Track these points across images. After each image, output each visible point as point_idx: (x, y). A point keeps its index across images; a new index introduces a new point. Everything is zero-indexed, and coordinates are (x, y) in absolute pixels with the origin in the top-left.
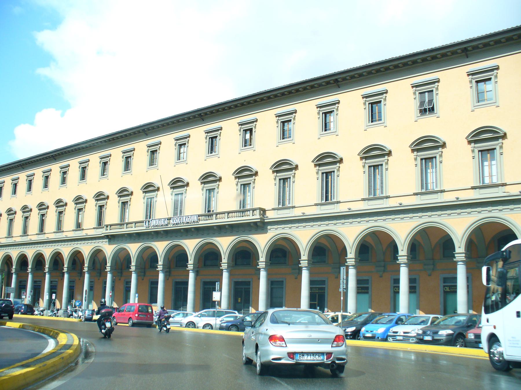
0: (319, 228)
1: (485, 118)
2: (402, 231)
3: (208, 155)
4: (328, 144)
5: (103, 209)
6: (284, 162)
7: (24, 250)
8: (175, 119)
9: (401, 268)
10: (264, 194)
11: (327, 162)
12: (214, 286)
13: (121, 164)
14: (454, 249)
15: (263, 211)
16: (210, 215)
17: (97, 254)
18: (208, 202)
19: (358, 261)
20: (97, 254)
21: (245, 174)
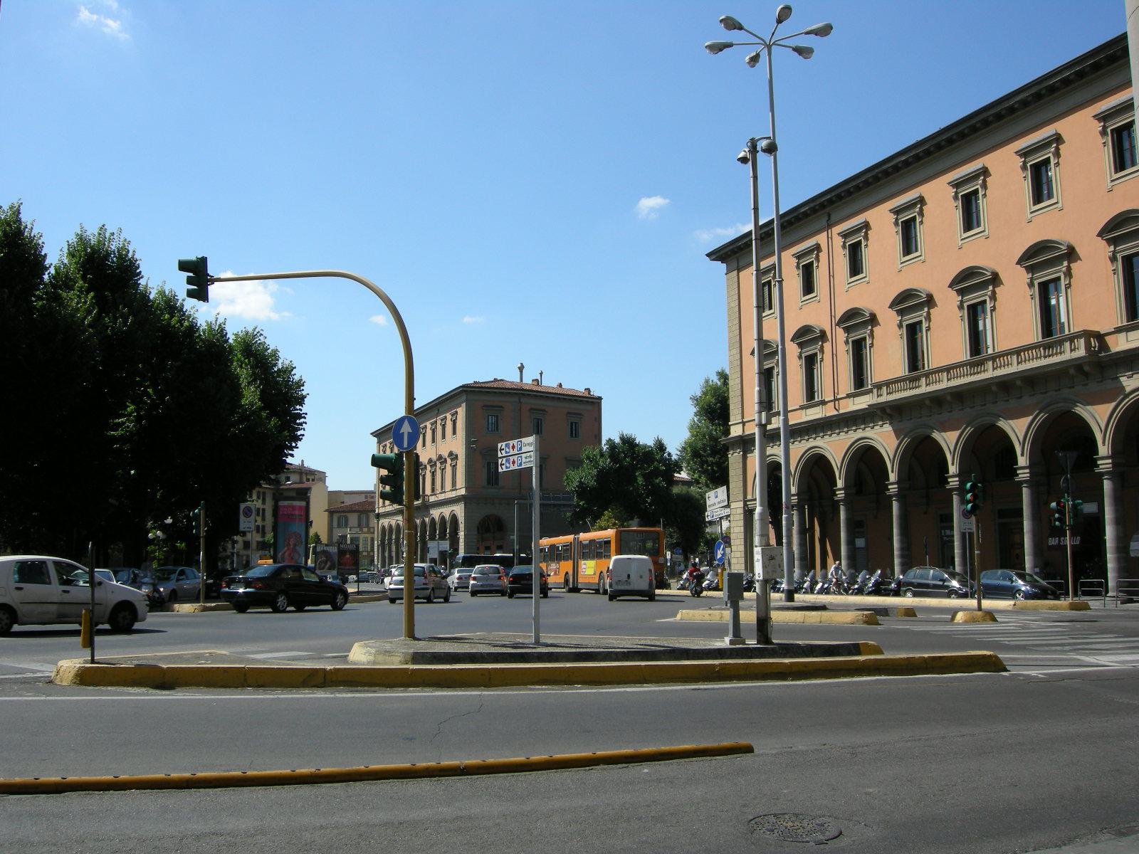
6: (852, 314)
7: (869, 433)
8: (833, 194)
11: (1046, 259)
13: (894, 239)
16: (981, 363)
17: (866, 458)
20: (866, 458)
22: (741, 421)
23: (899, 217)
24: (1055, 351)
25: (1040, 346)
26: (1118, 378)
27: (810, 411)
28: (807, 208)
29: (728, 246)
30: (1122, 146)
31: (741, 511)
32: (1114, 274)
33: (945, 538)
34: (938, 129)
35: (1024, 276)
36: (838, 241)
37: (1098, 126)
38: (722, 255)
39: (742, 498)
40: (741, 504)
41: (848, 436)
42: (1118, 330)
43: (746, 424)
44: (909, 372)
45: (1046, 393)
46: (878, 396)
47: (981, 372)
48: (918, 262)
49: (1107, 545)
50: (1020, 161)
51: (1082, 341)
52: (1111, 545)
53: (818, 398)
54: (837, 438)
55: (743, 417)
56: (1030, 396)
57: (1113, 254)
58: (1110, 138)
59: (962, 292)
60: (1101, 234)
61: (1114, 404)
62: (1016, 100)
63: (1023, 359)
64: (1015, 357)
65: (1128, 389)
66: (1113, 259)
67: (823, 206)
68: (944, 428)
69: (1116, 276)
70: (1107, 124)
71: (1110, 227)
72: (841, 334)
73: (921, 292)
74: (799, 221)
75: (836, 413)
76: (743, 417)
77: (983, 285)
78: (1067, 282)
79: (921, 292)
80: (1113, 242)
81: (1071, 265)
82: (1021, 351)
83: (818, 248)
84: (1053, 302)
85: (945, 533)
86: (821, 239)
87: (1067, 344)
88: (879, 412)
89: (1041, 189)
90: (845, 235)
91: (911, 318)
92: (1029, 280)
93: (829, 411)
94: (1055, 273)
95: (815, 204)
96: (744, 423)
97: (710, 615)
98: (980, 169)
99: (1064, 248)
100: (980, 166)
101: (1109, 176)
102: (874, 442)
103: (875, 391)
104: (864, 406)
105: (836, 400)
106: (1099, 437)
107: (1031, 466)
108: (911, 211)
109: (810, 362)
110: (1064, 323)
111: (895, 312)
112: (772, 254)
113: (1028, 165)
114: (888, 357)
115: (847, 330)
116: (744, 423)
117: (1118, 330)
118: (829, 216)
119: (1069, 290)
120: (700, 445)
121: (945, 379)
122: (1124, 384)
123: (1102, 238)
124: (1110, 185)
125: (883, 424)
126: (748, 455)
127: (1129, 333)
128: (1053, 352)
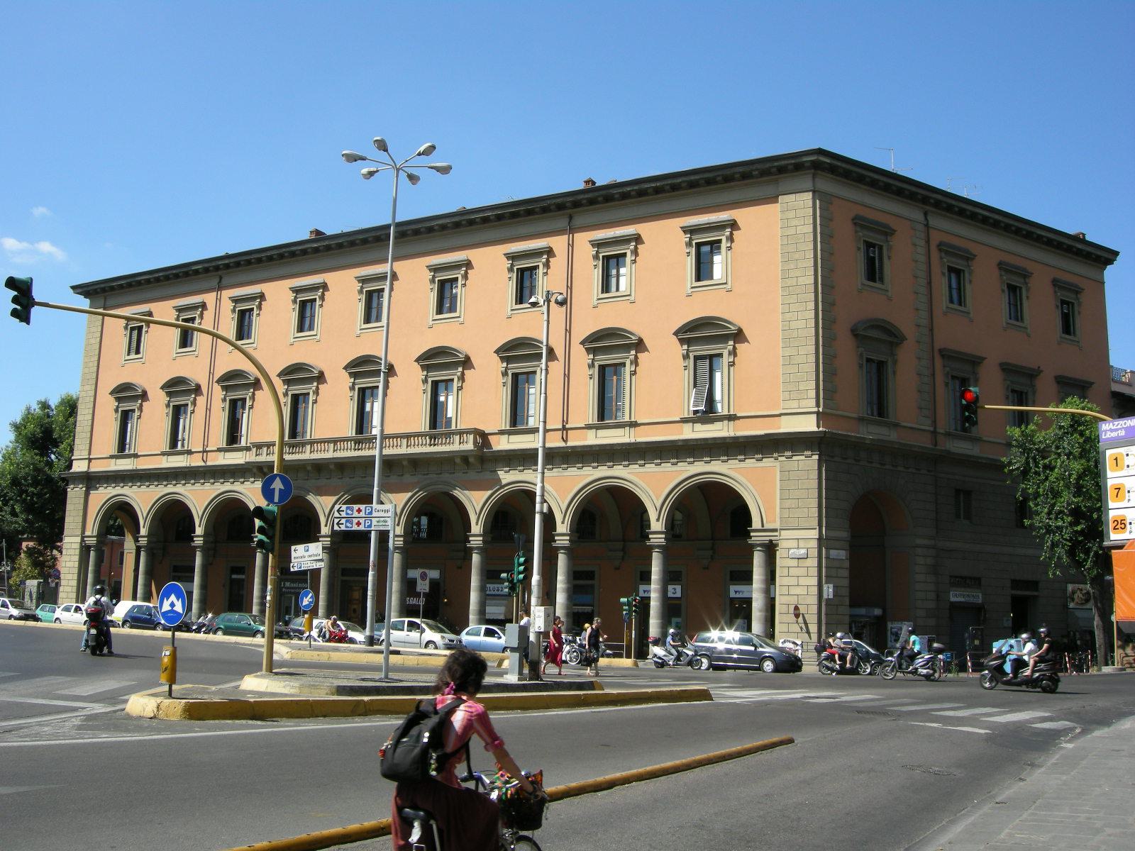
0: (165, 488)
1: (705, 305)
2: (654, 486)
3: (128, 358)
4: (371, 343)
5: (301, 406)
7: (237, 487)
9: (559, 555)
10: (479, 404)
11: (365, 370)
12: (363, 579)
14: (649, 526)
15: (483, 437)
18: (436, 409)
19: (490, 539)
21: (442, 364)
22: (87, 457)
23: (298, 296)
24: (367, 447)
25: (426, 436)
26: (496, 471)
27: (171, 458)
28: (200, 267)
29: (98, 284)
30: (444, 295)
31: (78, 546)
32: (504, 386)
33: (284, 590)
34: (340, 232)
35: (419, 374)
36: (227, 305)
37: (292, 296)
38: (89, 291)
39: (79, 532)
40: (78, 539)
41: (213, 487)
42: (502, 432)
43: (93, 461)
44: (356, 434)
45: (427, 474)
46: (257, 455)
47: (295, 453)
48: (456, 323)
49: (471, 608)
50: (508, 263)
51: (471, 437)
52: (475, 608)
53: (183, 446)
54: (201, 488)
55: (90, 454)
56: (412, 475)
57: (506, 370)
58: (694, 249)
59: (119, 400)
60: (497, 352)
61: (489, 492)
62: (437, 223)
63: (339, 448)
64: (405, 441)
65: (504, 482)
66: (505, 374)
67: (217, 268)
68: (320, 492)
69: (505, 388)
70: (436, 275)
71: (286, 372)
72: (218, 392)
73: (314, 368)
74: (417, 235)
75: (203, 464)
76: (90, 454)
77: (134, 398)
78: (633, 369)
79: (314, 368)
80: (355, 375)
81: (638, 354)
82: (325, 442)
83: (203, 306)
84: (442, 399)
85: (284, 584)
86: (210, 298)
87: (308, 447)
88: (255, 470)
89: (371, 312)
90: (236, 300)
91: (126, 406)
92: (424, 377)
93: (196, 461)
94: (621, 359)
95: (132, 280)
96: (90, 460)
97: (318, 655)
98: (259, 293)
99: (733, 328)
100: (320, 280)
101: (431, 317)
102: (244, 497)
103: (255, 449)
104: (241, 461)
105: (204, 451)
106: (653, 515)
107: (205, 535)
108: (313, 293)
109: (178, 412)
110: (451, 418)
111: (220, 387)
112: (386, 261)
113: (237, 309)
114: (264, 422)
115: (225, 388)
116: (90, 460)
117: (502, 432)
118: (221, 278)
119: (460, 392)
120: (22, 473)
121: (332, 449)
122: (501, 477)
123: (346, 371)
124: (510, 313)
125: (244, 481)
126: (91, 492)
127: (598, 431)
128: (362, 446)
